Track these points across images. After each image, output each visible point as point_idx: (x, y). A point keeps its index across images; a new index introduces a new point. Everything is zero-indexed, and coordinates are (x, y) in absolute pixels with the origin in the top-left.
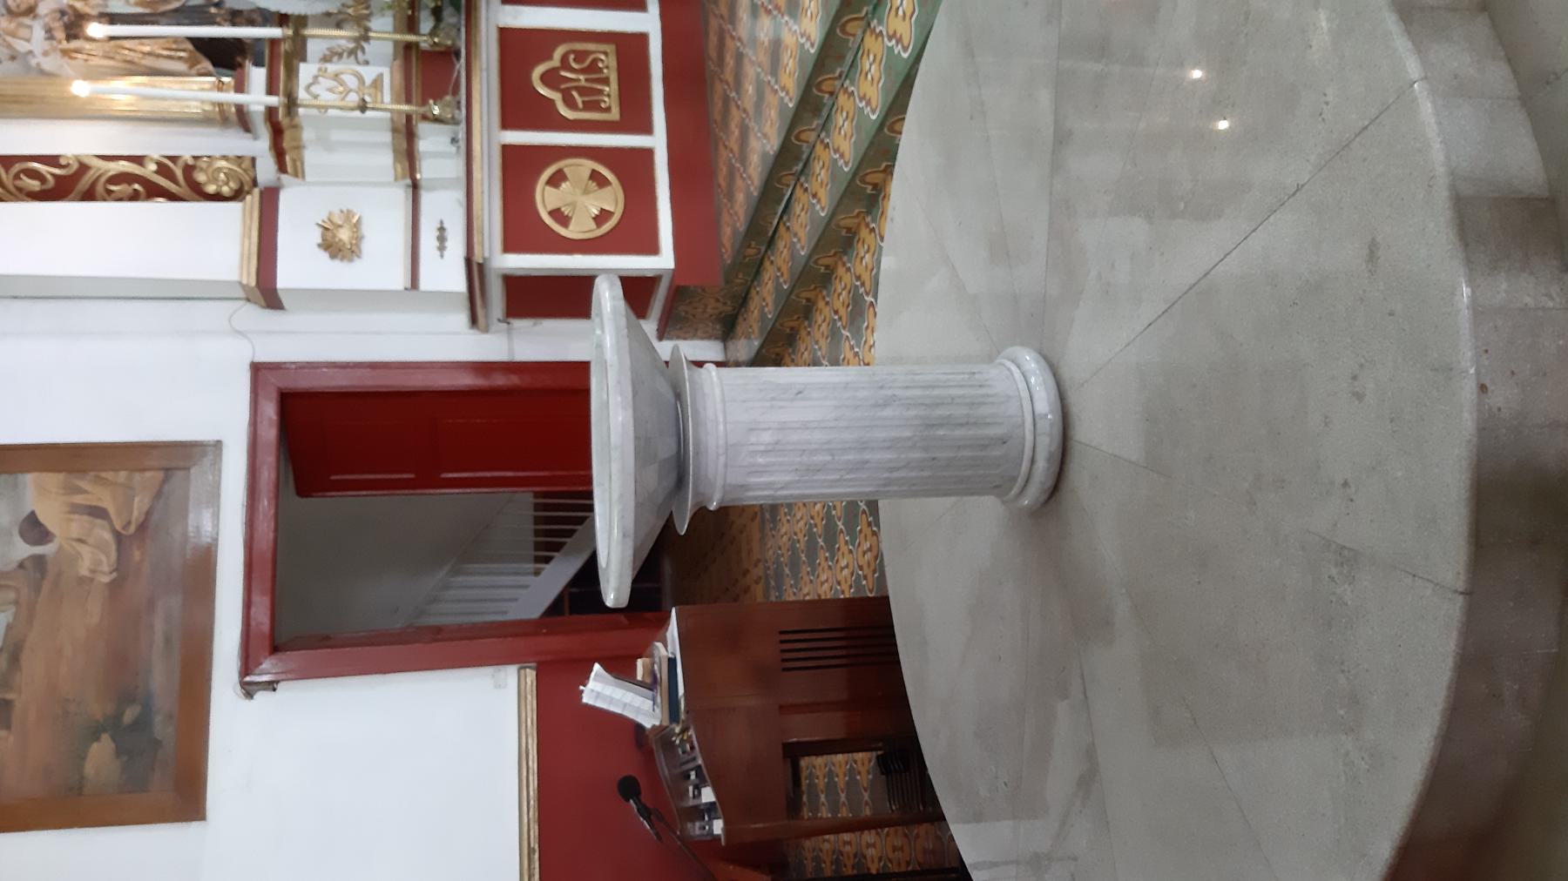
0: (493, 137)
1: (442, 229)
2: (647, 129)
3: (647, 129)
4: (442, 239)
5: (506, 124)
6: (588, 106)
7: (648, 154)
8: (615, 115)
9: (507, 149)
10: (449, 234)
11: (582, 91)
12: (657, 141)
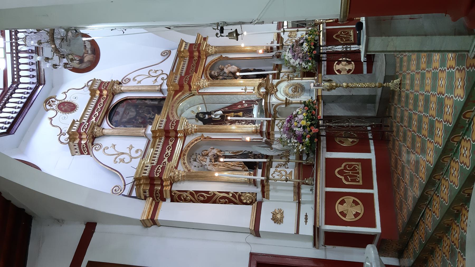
0: (323, 189)
1: (306, 216)
2: (372, 188)
3: (372, 188)
4: (306, 219)
5: (327, 186)
6: (352, 181)
7: (372, 195)
8: (361, 183)
9: (327, 193)
10: (308, 217)
11: (350, 176)
12: (375, 191)
